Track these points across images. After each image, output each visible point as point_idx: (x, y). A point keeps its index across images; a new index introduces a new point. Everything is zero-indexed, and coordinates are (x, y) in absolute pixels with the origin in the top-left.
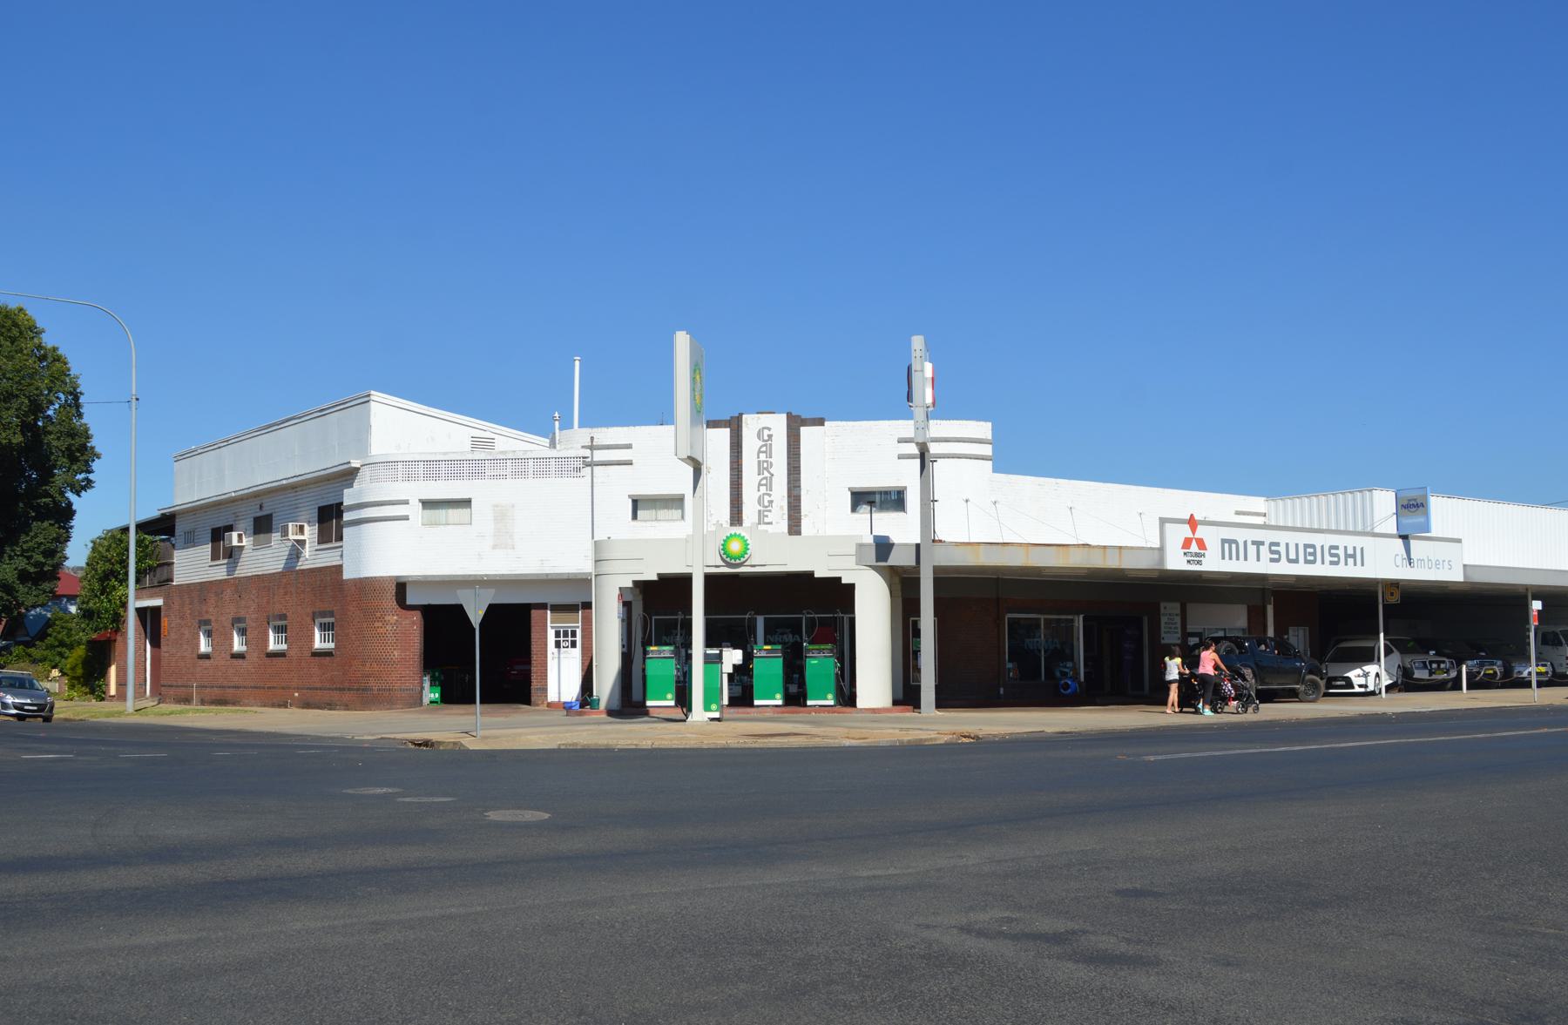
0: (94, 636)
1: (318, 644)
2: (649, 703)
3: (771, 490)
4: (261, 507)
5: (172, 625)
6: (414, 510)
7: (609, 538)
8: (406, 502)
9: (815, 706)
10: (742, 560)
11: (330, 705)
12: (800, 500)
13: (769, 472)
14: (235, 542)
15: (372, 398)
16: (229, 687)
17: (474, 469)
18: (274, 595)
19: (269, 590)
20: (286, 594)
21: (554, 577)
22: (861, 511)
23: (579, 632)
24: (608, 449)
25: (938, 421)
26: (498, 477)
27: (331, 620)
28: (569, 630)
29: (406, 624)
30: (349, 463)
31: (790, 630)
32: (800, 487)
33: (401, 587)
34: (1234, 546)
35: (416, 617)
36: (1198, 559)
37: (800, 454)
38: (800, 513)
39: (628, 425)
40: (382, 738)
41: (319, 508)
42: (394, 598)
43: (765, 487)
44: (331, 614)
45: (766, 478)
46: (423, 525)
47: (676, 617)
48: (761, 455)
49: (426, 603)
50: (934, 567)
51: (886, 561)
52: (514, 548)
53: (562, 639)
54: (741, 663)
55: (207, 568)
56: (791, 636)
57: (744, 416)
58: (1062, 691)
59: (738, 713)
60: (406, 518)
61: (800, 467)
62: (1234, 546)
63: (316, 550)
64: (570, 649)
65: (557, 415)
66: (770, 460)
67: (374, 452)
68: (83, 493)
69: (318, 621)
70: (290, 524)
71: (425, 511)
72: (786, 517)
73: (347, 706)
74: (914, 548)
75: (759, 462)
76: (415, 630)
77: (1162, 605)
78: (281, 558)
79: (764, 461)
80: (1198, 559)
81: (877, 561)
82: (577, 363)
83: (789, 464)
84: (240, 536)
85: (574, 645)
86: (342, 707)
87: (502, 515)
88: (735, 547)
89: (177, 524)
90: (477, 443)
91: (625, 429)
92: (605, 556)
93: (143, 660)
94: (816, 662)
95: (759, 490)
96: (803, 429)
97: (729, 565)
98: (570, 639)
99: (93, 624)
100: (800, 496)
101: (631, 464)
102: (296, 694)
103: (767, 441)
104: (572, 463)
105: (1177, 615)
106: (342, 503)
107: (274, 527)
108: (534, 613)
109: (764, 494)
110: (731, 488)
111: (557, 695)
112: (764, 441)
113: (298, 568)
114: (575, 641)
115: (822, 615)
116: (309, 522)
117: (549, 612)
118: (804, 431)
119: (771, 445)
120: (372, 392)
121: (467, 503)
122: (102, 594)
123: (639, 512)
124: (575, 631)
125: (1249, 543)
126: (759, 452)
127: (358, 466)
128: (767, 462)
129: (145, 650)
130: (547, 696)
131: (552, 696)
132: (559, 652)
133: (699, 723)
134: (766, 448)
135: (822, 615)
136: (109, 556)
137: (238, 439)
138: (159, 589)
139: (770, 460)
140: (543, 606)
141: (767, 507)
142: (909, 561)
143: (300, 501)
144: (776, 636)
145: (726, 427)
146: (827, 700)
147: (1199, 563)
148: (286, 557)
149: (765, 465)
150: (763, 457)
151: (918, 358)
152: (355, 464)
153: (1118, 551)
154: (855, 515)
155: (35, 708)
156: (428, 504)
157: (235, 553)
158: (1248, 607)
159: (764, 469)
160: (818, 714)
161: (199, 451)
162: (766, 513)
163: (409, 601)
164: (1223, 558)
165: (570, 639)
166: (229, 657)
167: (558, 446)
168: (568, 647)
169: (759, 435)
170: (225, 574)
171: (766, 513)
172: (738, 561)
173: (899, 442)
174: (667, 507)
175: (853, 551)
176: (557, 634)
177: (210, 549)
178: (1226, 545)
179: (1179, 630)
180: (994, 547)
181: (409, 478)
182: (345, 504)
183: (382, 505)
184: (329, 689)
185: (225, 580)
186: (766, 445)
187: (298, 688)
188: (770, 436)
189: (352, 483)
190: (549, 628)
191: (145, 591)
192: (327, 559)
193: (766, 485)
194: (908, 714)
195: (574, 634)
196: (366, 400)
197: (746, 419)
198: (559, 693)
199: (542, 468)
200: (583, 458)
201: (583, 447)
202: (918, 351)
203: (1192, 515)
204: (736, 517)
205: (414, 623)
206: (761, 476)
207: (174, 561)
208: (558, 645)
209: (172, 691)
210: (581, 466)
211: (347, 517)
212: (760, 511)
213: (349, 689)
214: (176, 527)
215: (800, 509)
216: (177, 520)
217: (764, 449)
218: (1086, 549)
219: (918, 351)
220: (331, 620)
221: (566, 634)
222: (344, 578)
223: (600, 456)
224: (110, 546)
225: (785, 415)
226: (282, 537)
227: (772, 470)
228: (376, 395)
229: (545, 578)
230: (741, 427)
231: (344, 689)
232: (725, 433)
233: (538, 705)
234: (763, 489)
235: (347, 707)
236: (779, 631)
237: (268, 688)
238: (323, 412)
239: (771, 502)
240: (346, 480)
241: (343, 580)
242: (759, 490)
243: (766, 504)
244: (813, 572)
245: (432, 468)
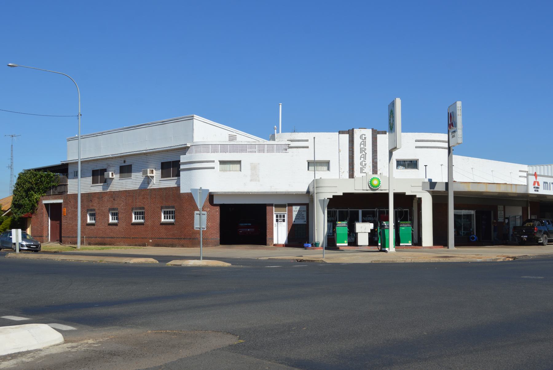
0: (23, 215)
1: (111, 221)
3: (365, 159)
4: (125, 162)
5: (69, 211)
6: (217, 165)
7: (321, 178)
8: (213, 161)
9: (403, 246)
10: (378, 188)
11: (172, 245)
13: (365, 152)
14: (110, 176)
15: (194, 118)
16: (107, 238)
17: (242, 148)
18: (136, 199)
19: (133, 197)
20: (144, 198)
22: (399, 168)
24: (299, 141)
26: (252, 152)
27: (173, 210)
28: (282, 215)
29: (213, 212)
30: (186, 144)
31: (372, 215)
32: (377, 158)
33: (211, 196)
34: (547, 184)
35: (218, 209)
36: (537, 189)
37: (377, 145)
38: (377, 169)
39: (306, 132)
40: (269, 259)
41: (161, 163)
42: (208, 201)
43: (363, 158)
44: (173, 207)
45: (363, 155)
46: (220, 171)
47: (347, 210)
49: (222, 203)
50: (454, 191)
51: (434, 189)
52: (259, 181)
53: (279, 218)
54: (373, 228)
55: (90, 187)
57: (355, 130)
58: (471, 240)
60: (213, 168)
62: (547, 184)
63: (160, 180)
65: (275, 127)
66: (365, 147)
67: (195, 141)
69: (163, 210)
70: (148, 169)
71: (220, 165)
72: (371, 170)
73: (183, 245)
74: (444, 185)
75: (361, 148)
76: (217, 214)
77: (499, 206)
78: (137, 185)
79: (363, 148)
80: (537, 189)
82: (281, 106)
83: (372, 149)
84: (112, 174)
85: (284, 221)
86: (180, 246)
87: (254, 168)
88: (375, 182)
89: (69, 168)
90: (232, 138)
91: (305, 133)
92: (320, 185)
93: (47, 226)
94: (404, 228)
95: (360, 159)
96: (378, 136)
97: (372, 189)
98: (282, 218)
99: (21, 210)
100: (377, 162)
102: (151, 241)
103: (364, 140)
104: (283, 147)
105: (502, 210)
106: (179, 161)
107: (132, 170)
108: (268, 208)
109: (363, 161)
110: (349, 158)
111: (277, 241)
113: (148, 188)
114: (276, 217)
115: (363, 210)
116: (155, 169)
117: (274, 207)
118: (379, 136)
119: (365, 141)
120: (194, 115)
121: (239, 162)
122: (26, 197)
123: (310, 167)
124: (284, 215)
125: (551, 183)
126: (361, 144)
127: (189, 146)
128: (364, 148)
129: (48, 222)
130: (273, 242)
131: (275, 242)
132: (278, 224)
133: (393, 252)
134: (364, 143)
135: (363, 210)
136: (31, 181)
137: (109, 133)
138: (58, 195)
139: (365, 147)
140: (271, 205)
141: (364, 166)
142: (443, 189)
143: (150, 160)
145: (347, 134)
146: (409, 243)
147: (538, 191)
148: (141, 183)
150: (362, 146)
151: (459, 110)
152: (188, 145)
153: (515, 186)
154: (398, 170)
155: (35, 247)
156: (222, 162)
157: (108, 181)
158: (522, 207)
159: (363, 151)
161: (84, 137)
162: (363, 169)
163: (215, 203)
164: (544, 189)
165: (282, 218)
166: (107, 225)
167: (276, 140)
168: (281, 222)
169: (361, 137)
170: (102, 189)
171: (363, 169)
172: (376, 188)
173: (416, 141)
174: (322, 166)
175: (421, 185)
176: (277, 216)
177: (92, 179)
178: (545, 184)
179: (503, 216)
180: (475, 184)
181: (214, 151)
182: (181, 162)
183: (202, 162)
184: (173, 239)
185: (101, 192)
186: (363, 141)
187: (152, 238)
188: (365, 138)
189: (186, 153)
190: (274, 214)
191: (50, 197)
192: (170, 183)
193: (363, 157)
194: (440, 249)
195: (284, 216)
196: (192, 118)
197: (356, 131)
198: (278, 240)
199: (271, 149)
200: (288, 145)
201: (288, 140)
202: (459, 107)
203: (535, 172)
204: (375, 171)
205: (217, 211)
206: (362, 154)
207: (68, 183)
208: (277, 221)
209: (69, 240)
210: (287, 148)
211: (182, 167)
212: (361, 168)
213: (184, 239)
214: (69, 169)
216: (69, 166)
217: (363, 143)
218: (506, 185)
219: (459, 107)
220: (173, 210)
221: (280, 216)
222: (181, 192)
223: (293, 144)
224: (31, 177)
226: (143, 175)
228: (196, 117)
229: (276, 194)
231: (181, 239)
232: (346, 137)
233: (269, 245)
234: (362, 159)
235: (183, 246)
236: (368, 216)
237: (132, 238)
238: (163, 123)
239: (365, 164)
240: (178, 152)
241: (180, 193)
242: (360, 159)
243: (364, 165)
244: (405, 193)
245: (224, 148)
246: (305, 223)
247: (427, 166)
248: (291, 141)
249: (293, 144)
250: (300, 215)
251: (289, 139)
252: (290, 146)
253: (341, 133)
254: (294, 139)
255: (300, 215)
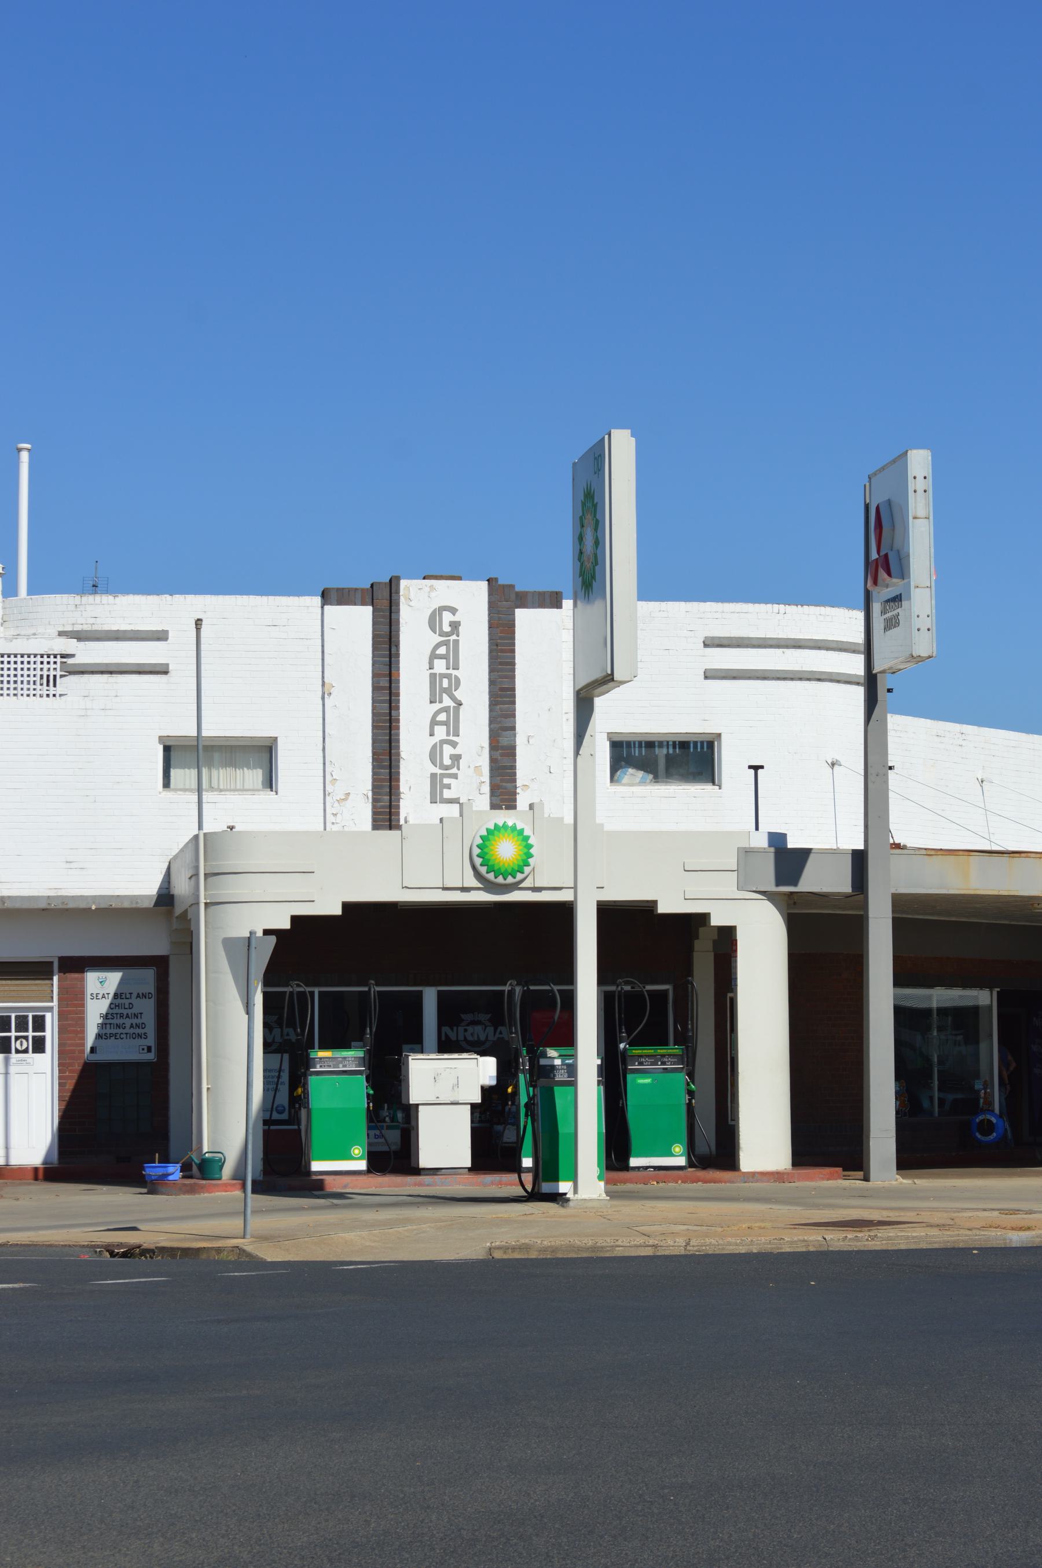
2: (316, 1166)
7: (231, 828)
10: (519, 876)
12: (514, 755)
13: (453, 698)
21: (18, 905)
23: (51, 1021)
25: (782, 606)
32: (513, 728)
37: (513, 664)
38: (515, 781)
39: (158, 592)
45: (446, 710)
48: (436, 662)
51: (796, 884)
54: (494, 1082)
56: (490, 1030)
57: (403, 583)
59: (500, 1183)
61: (513, 689)
64: (30, 1055)
66: (454, 672)
68: (631, 774)
72: (486, 789)
75: (433, 676)
79: (443, 676)
81: (778, 884)
82: (25, 456)
85: (39, 1046)
88: (506, 851)
91: (153, 599)
94: (648, 1081)
95: (432, 734)
97: (489, 886)
98: (30, 1034)
101: (166, 673)
103: (448, 634)
104: (39, 666)
109: (443, 742)
110: (374, 727)
112: (442, 634)
118: (522, 615)
119: (456, 642)
124: (43, 1017)
126: (433, 656)
128: (448, 676)
132: (7, 1062)
139: (454, 672)
142: (840, 883)
144: (461, 1029)
145: (363, 604)
146: (673, 1155)
149: (445, 683)
150: (440, 666)
160: (661, 1185)
162: (446, 781)
165: (30, 1034)
168: (26, 1051)
169: (434, 621)
171: (446, 781)
172: (510, 880)
175: (732, 862)
180: (995, 859)
186: (446, 643)
188: (455, 626)
195: (39, 1024)
197: (408, 588)
200: (63, 656)
201: (61, 634)
202: (920, 478)
206: (437, 706)
210: (58, 673)
212: (433, 776)
215: (515, 774)
217: (442, 650)
219: (920, 478)
223: (87, 653)
225: (484, 585)
227: (458, 694)
230: (398, 605)
234: (441, 732)
236: (467, 1017)
239: (456, 758)
242: (432, 734)
243: (447, 761)
244: (655, 902)
246: (151, 1057)
247: (762, 767)
248: (80, 636)
249: (87, 653)
250: (122, 1016)
251: (69, 628)
252: (70, 661)
253: (334, 596)
254: (95, 628)
255: (122, 1016)
